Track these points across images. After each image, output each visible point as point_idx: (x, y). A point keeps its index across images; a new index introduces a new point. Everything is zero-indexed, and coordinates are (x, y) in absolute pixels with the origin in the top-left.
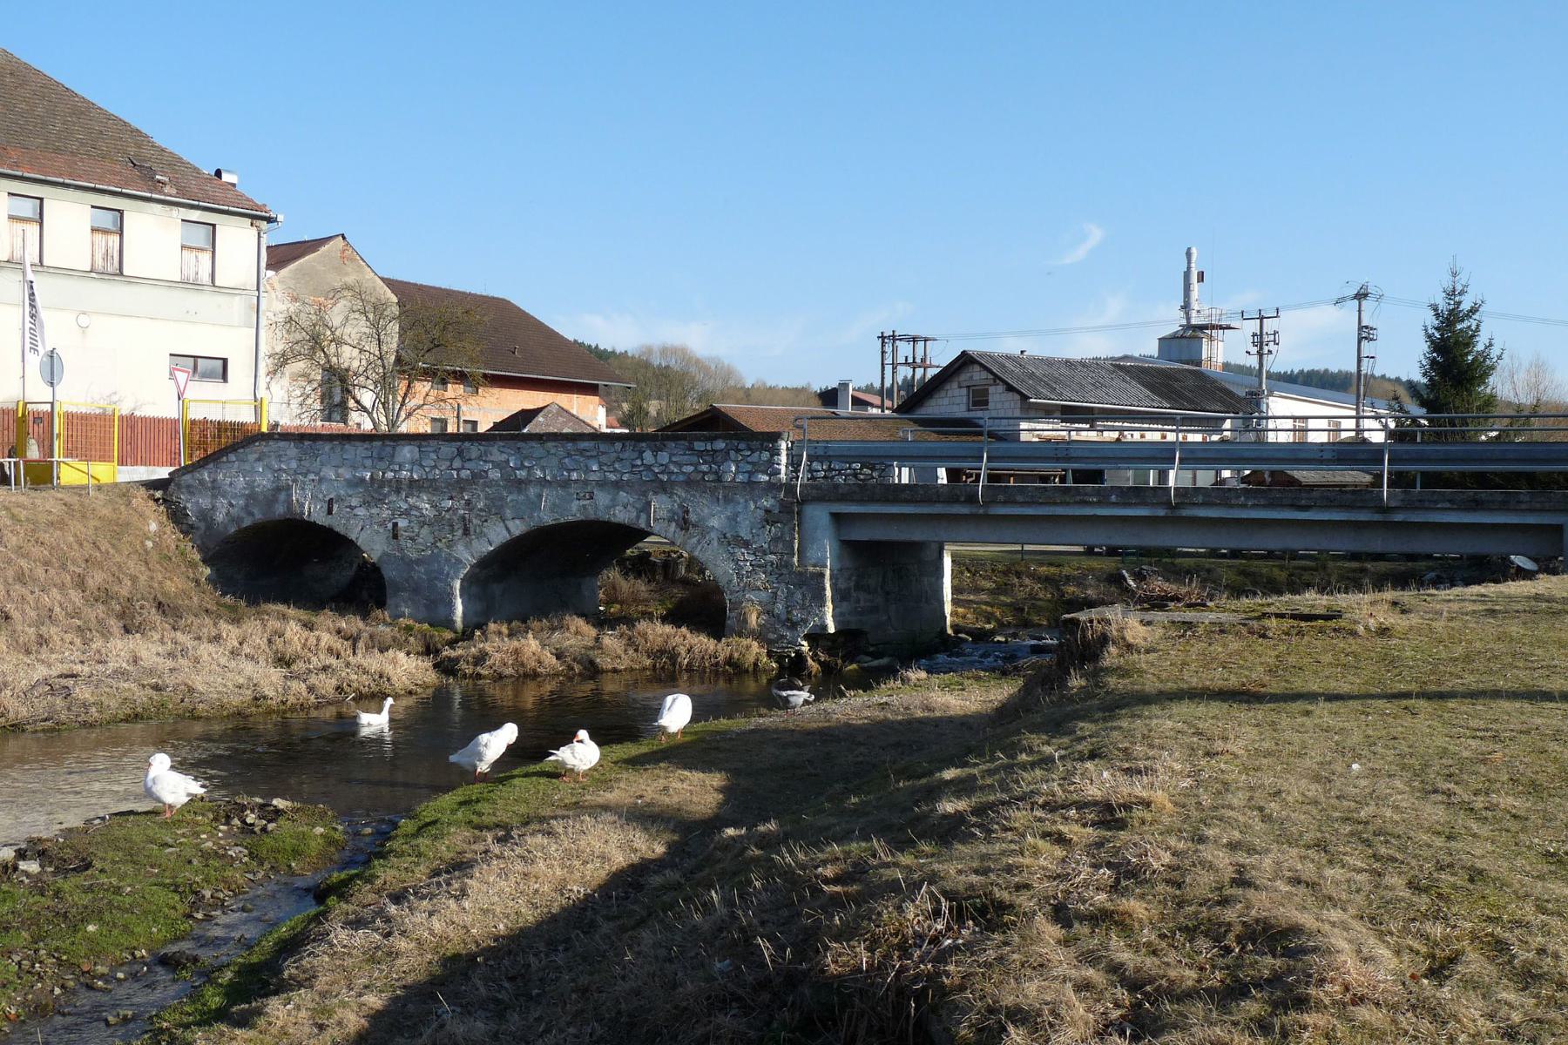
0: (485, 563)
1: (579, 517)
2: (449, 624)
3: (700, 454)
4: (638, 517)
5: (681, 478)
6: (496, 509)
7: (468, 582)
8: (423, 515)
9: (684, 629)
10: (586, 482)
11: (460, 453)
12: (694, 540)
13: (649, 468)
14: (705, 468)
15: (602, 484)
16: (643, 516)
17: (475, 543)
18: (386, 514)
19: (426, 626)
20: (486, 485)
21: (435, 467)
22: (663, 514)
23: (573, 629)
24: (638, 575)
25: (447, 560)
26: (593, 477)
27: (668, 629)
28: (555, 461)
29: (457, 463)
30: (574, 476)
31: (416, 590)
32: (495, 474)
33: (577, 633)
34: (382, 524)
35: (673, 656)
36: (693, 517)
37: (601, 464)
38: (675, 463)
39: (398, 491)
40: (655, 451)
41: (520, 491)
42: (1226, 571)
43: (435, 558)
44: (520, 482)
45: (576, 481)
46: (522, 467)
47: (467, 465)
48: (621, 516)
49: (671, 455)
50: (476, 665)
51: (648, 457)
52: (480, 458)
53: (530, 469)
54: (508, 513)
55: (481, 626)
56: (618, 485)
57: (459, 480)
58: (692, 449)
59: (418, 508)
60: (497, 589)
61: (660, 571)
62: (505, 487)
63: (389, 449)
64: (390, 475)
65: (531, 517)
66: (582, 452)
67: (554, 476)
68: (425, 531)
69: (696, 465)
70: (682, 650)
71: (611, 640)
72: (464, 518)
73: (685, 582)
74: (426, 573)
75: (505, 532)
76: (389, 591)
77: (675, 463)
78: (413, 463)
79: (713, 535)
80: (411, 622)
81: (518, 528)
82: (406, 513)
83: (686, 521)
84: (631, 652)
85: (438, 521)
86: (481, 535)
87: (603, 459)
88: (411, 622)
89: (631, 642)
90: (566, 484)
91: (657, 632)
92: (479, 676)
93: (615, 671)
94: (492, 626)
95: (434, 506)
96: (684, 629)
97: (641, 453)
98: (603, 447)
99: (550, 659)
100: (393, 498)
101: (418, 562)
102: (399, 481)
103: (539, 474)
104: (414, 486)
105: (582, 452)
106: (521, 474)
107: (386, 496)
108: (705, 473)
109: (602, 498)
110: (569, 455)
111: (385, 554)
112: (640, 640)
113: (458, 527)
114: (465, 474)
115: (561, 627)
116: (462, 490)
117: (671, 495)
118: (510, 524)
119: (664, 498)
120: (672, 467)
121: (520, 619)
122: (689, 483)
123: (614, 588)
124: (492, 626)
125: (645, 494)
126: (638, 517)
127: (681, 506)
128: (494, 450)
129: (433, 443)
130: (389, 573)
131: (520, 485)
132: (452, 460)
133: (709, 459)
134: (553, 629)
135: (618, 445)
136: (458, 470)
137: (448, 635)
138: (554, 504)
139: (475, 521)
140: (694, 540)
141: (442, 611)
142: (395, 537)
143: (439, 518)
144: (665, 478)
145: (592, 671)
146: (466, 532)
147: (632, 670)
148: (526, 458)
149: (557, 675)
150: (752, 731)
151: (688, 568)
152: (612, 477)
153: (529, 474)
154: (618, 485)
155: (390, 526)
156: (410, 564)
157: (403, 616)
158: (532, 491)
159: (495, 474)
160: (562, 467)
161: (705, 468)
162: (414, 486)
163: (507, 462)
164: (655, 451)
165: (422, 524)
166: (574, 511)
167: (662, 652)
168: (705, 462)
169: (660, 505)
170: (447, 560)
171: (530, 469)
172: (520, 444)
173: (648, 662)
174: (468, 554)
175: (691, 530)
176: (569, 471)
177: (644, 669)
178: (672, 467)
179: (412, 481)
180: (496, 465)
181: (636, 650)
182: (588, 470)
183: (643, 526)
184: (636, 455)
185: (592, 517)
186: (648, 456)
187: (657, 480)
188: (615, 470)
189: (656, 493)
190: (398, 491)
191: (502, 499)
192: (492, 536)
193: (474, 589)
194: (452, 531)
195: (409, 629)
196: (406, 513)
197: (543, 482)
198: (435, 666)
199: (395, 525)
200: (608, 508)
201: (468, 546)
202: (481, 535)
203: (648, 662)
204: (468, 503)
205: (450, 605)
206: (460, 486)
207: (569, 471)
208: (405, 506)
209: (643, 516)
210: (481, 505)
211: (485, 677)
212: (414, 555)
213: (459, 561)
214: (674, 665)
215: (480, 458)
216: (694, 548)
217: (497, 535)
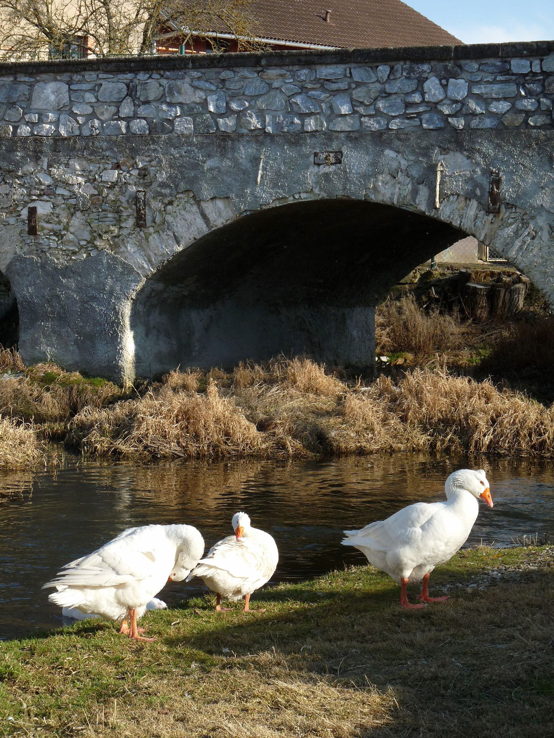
0: (171, 273)
1: (319, 194)
2: (113, 373)
3: (522, 79)
4: (415, 192)
5: (488, 123)
6: (186, 185)
7: (145, 304)
8: (74, 195)
9: (487, 384)
10: (330, 135)
11: (131, 91)
12: (509, 231)
13: (434, 107)
14: (528, 104)
15: (355, 137)
16: (423, 191)
17: (154, 239)
18: (19, 193)
19: (76, 375)
20: (170, 143)
21: (93, 115)
22: (459, 186)
23: (301, 380)
24: (447, 307)
25: (111, 268)
26: (341, 125)
27: (462, 383)
28: (279, 101)
29: (126, 109)
30: (311, 124)
31: (62, 318)
32: (184, 126)
33: (309, 385)
34: (13, 210)
35: (465, 430)
36: (507, 191)
37: (354, 103)
38: (479, 98)
39: (36, 157)
40: (445, 78)
41: (223, 152)
42: (319, 597)
43: (92, 263)
44: (225, 137)
45: (313, 134)
46: (229, 112)
47: (142, 111)
48: (388, 191)
49: (472, 83)
50: (116, 435)
51: (433, 88)
52: (161, 99)
53: (240, 114)
54: (206, 192)
55: (159, 379)
56: (381, 139)
57: (130, 136)
58: (507, 72)
59: (66, 184)
60: (196, 319)
61: (483, 302)
62: (201, 146)
63: (23, 89)
64: (25, 130)
65: (241, 195)
66: (322, 83)
67: (278, 126)
68: (77, 221)
69: (513, 99)
70: (482, 421)
71: (363, 403)
72: (136, 199)
73: (520, 317)
74: (79, 289)
75: (200, 222)
76: (23, 319)
77: (479, 98)
78: (59, 110)
79: (542, 221)
80: (55, 369)
81: (221, 214)
82: (49, 193)
83: (495, 198)
84: (394, 421)
85: (93, 206)
86: (163, 226)
87: (359, 94)
88: (55, 369)
89: (395, 404)
90: (297, 138)
91: (438, 387)
92: (117, 455)
93: (361, 452)
94: (176, 377)
95: (91, 181)
96: (487, 384)
97: (421, 81)
98: (358, 74)
99: (245, 430)
100: (30, 168)
101: (66, 271)
102: (38, 140)
103: (255, 122)
104: (62, 147)
105: (322, 83)
106: (227, 124)
107: (18, 165)
108: (528, 113)
109: (356, 160)
110: (303, 90)
111: (18, 259)
112: (411, 402)
113: (128, 212)
114: (139, 125)
115: (288, 380)
116: (134, 152)
117: (471, 153)
118: (208, 208)
119: (459, 158)
120: (473, 105)
121: (224, 364)
122: (501, 131)
123: (406, 328)
124: (176, 377)
125: (426, 152)
126: (415, 192)
127: (487, 172)
128: (185, 85)
129: (90, 76)
130: (25, 290)
131: (224, 142)
132: (118, 104)
133: (535, 87)
134: (271, 382)
135: (383, 70)
136: (128, 119)
137: (108, 389)
138: (278, 174)
139: (156, 205)
140: (509, 231)
141: (102, 351)
142: (33, 231)
143: (98, 200)
144: (460, 123)
145: (322, 449)
146: (140, 222)
147: (392, 451)
148: (233, 97)
149: (256, 456)
150: (528, 577)
151: (529, 297)
152: (373, 125)
153: (238, 124)
154: (381, 139)
155: (25, 213)
156: (54, 274)
157: (43, 359)
158: (244, 152)
159: (184, 126)
160: (291, 110)
161: (528, 104)
162: (62, 147)
163: (205, 104)
164: (445, 78)
165: (73, 210)
166: (310, 184)
167: (447, 422)
168: (530, 94)
169: (452, 169)
170: (111, 268)
171: (240, 114)
172: (226, 74)
173: (422, 439)
174: (143, 257)
175: (504, 213)
176: (303, 116)
177: (416, 450)
178: (473, 105)
179: (57, 139)
180: (188, 110)
181: (404, 419)
182: (333, 115)
183: (423, 207)
184: (411, 85)
185: (339, 193)
186: (433, 88)
187: (446, 128)
188: (378, 113)
189: (445, 150)
190: (36, 157)
191: (196, 166)
192: (180, 228)
193: (156, 318)
194: (118, 221)
195: (47, 381)
196: (49, 193)
197: (260, 137)
198: (40, 436)
199: (33, 211)
200: (365, 177)
201: (142, 246)
202: (163, 226)
203: (422, 439)
204: (143, 174)
205: (115, 340)
206: (132, 145)
207: (303, 116)
208: (47, 181)
209: (423, 191)
210: (162, 177)
211: (126, 457)
212: (60, 261)
213: (128, 270)
214: (466, 445)
215: (161, 99)
216: (509, 245)
217: (188, 226)
